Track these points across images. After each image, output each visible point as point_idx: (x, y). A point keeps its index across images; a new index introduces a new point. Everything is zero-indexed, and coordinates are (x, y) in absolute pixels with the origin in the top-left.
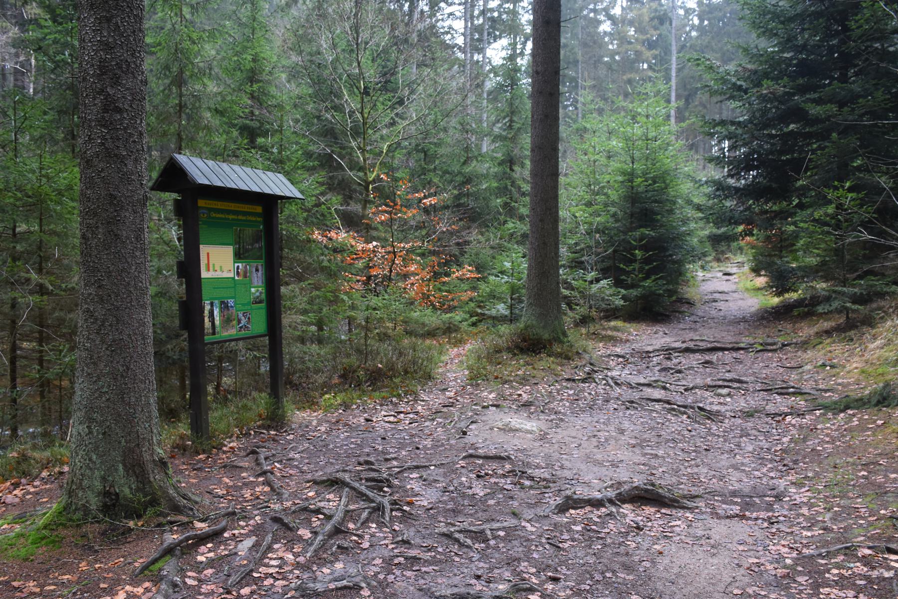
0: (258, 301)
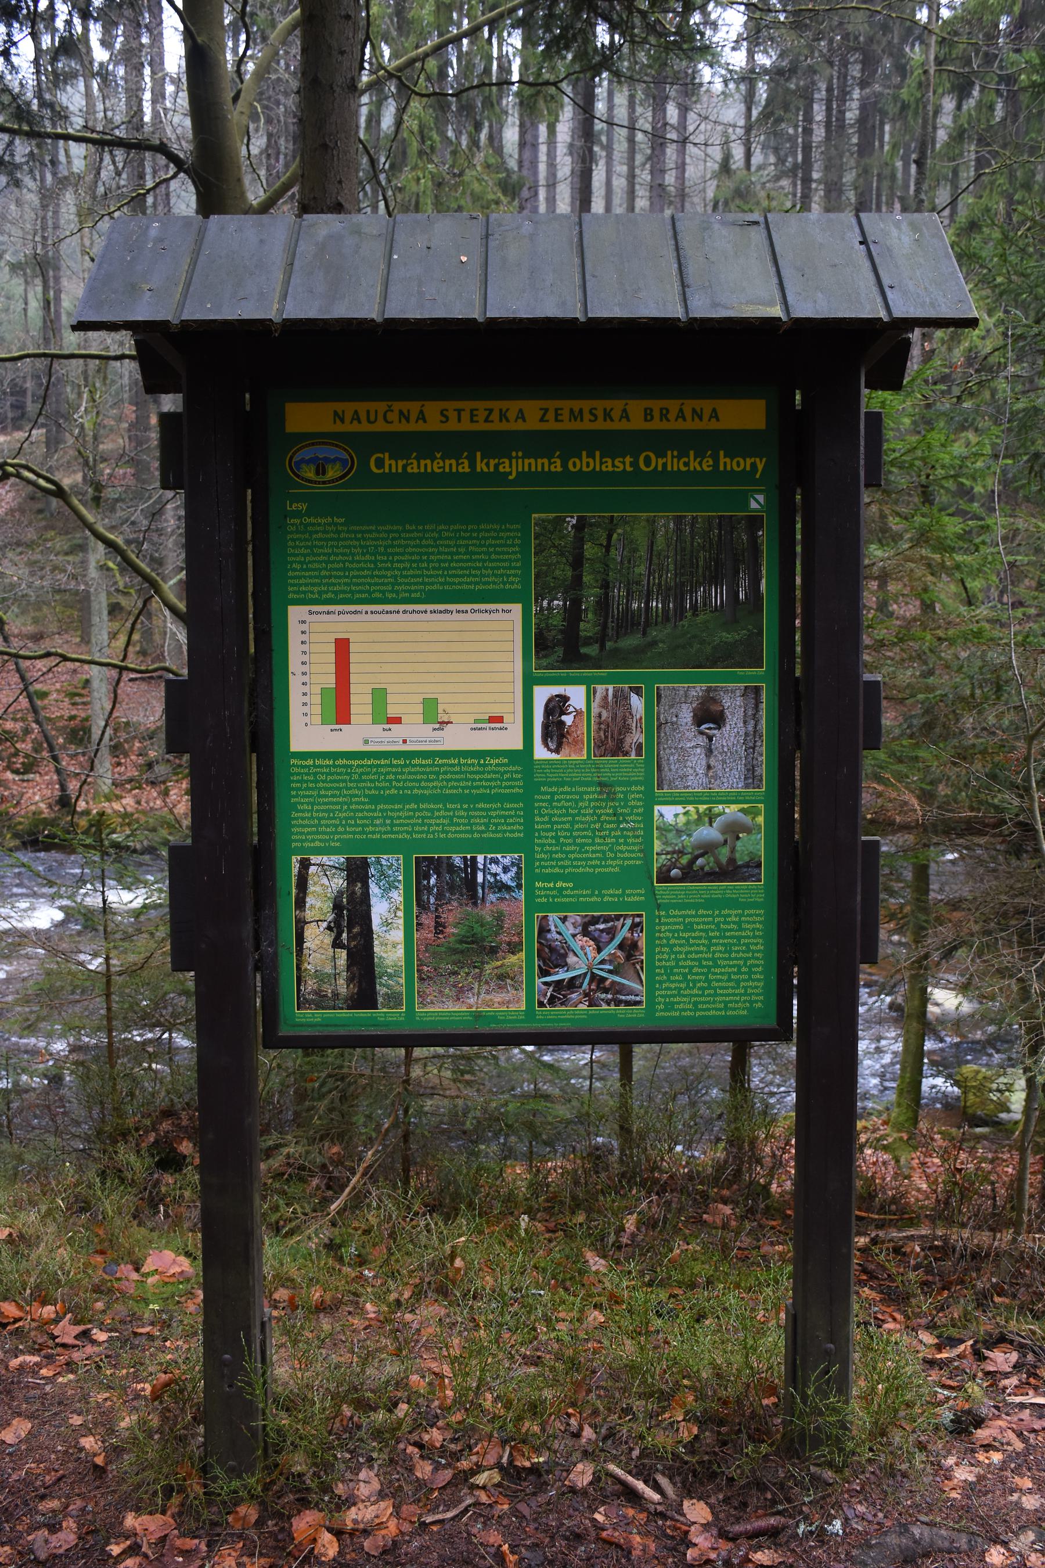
0: (705, 867)
